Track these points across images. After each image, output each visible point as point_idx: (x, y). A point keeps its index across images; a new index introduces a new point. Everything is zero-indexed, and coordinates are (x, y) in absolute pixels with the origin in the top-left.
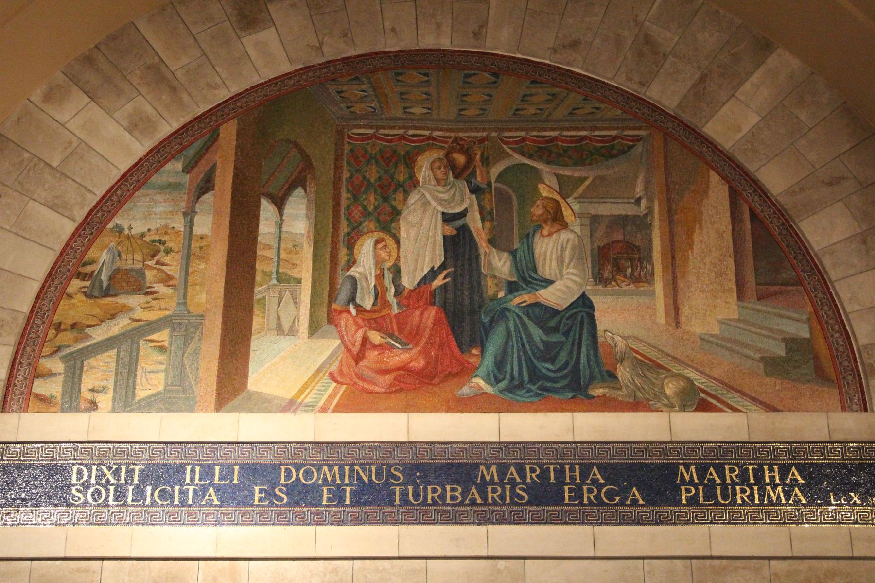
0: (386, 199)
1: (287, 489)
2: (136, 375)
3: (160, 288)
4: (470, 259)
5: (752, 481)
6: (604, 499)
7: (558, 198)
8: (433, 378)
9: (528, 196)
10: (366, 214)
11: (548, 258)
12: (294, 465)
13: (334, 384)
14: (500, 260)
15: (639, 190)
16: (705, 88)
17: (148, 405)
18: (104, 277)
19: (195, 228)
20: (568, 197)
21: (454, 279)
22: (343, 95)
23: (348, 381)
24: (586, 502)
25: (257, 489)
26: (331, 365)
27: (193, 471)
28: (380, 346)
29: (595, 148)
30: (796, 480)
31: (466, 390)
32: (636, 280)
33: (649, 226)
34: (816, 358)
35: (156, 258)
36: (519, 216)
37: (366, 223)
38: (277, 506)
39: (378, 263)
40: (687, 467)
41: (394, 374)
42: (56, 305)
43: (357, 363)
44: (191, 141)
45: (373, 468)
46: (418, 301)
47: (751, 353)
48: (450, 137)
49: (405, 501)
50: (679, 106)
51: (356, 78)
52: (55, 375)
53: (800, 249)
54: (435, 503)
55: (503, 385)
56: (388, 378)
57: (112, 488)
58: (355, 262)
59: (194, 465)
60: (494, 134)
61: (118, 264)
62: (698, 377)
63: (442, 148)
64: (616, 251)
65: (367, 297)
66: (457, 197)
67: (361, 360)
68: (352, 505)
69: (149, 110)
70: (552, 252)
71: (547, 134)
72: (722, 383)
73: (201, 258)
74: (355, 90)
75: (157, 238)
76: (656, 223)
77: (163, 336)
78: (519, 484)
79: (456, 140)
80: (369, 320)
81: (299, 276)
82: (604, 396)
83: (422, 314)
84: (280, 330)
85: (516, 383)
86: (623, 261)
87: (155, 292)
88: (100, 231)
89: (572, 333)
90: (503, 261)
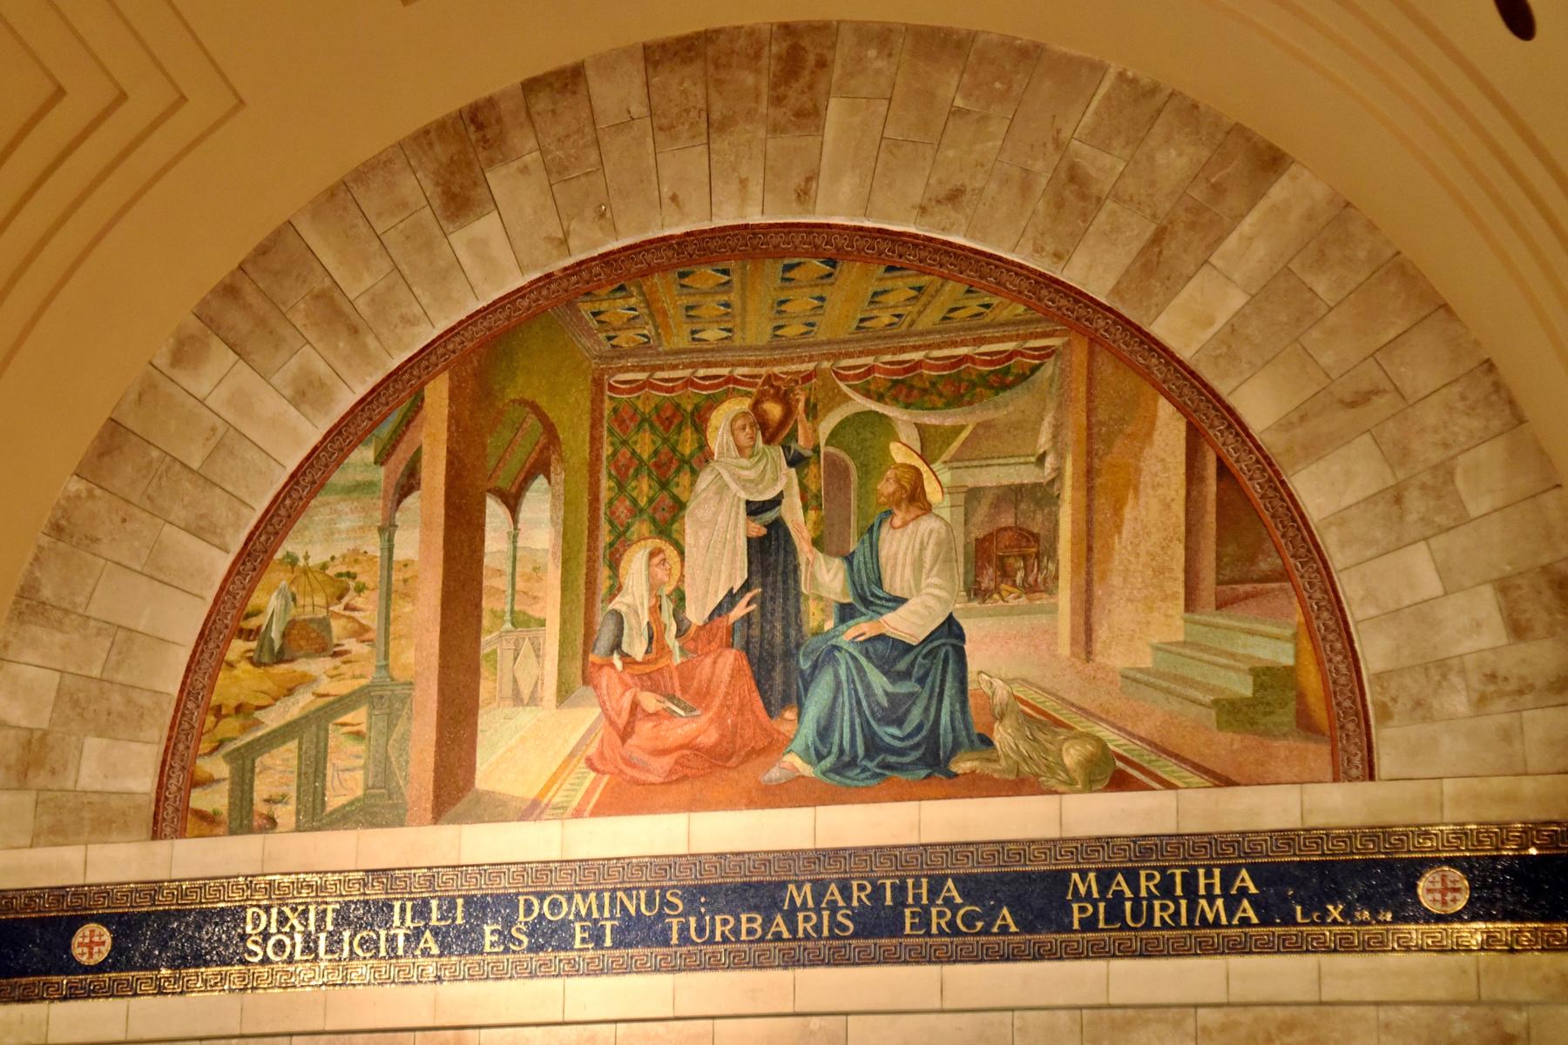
0: (664, 485)
3: (351, 645)
5: (1179, 892)
7: (919, 463)
8: (729, 758)
10: (636, 511)
11: (900, 562)
12: (536, 894)
15: (1044, 441)
16: (1160, 252)
17: (344, 819)
20: (934, 461)
21: (762, 606)
22: (602, 318)
23: (611, 768)
24: (934, 930)
28: (656, 714)
32: (1030, 589)
33: (1055, 500)
34: (1301, 697)
35: (345, 601)
36: (860, 499)
39: (654, 587)
41: (675, 755)
42: (214, 678)
43: (624, 741)
45: (643, 894)
47: (1199, 695)
48: (759, 376)
49: (685, 939)
51: (622, 288)
52: (218, 781)
55: (828, 763)
56: (667, 761)
58: (620, 589)
60: (826, 365)
61: (293, 612)
63: (748, 394)
65: (637, 641)
66: (769, 475)
69: (322, 367)
72: (1150, 743)
73: (406, 596)
75: (344, 569)
76: (1067, 494)
77: (358, 717)
79: (769, 379)
81: (542, 616)
82: (973, 772)
83: (715, 662)
84: (517, 699)
85: (846, 758)
86: (1011, 560)
87: (346, 652)
88: (265, 565)
89: (930, 679)
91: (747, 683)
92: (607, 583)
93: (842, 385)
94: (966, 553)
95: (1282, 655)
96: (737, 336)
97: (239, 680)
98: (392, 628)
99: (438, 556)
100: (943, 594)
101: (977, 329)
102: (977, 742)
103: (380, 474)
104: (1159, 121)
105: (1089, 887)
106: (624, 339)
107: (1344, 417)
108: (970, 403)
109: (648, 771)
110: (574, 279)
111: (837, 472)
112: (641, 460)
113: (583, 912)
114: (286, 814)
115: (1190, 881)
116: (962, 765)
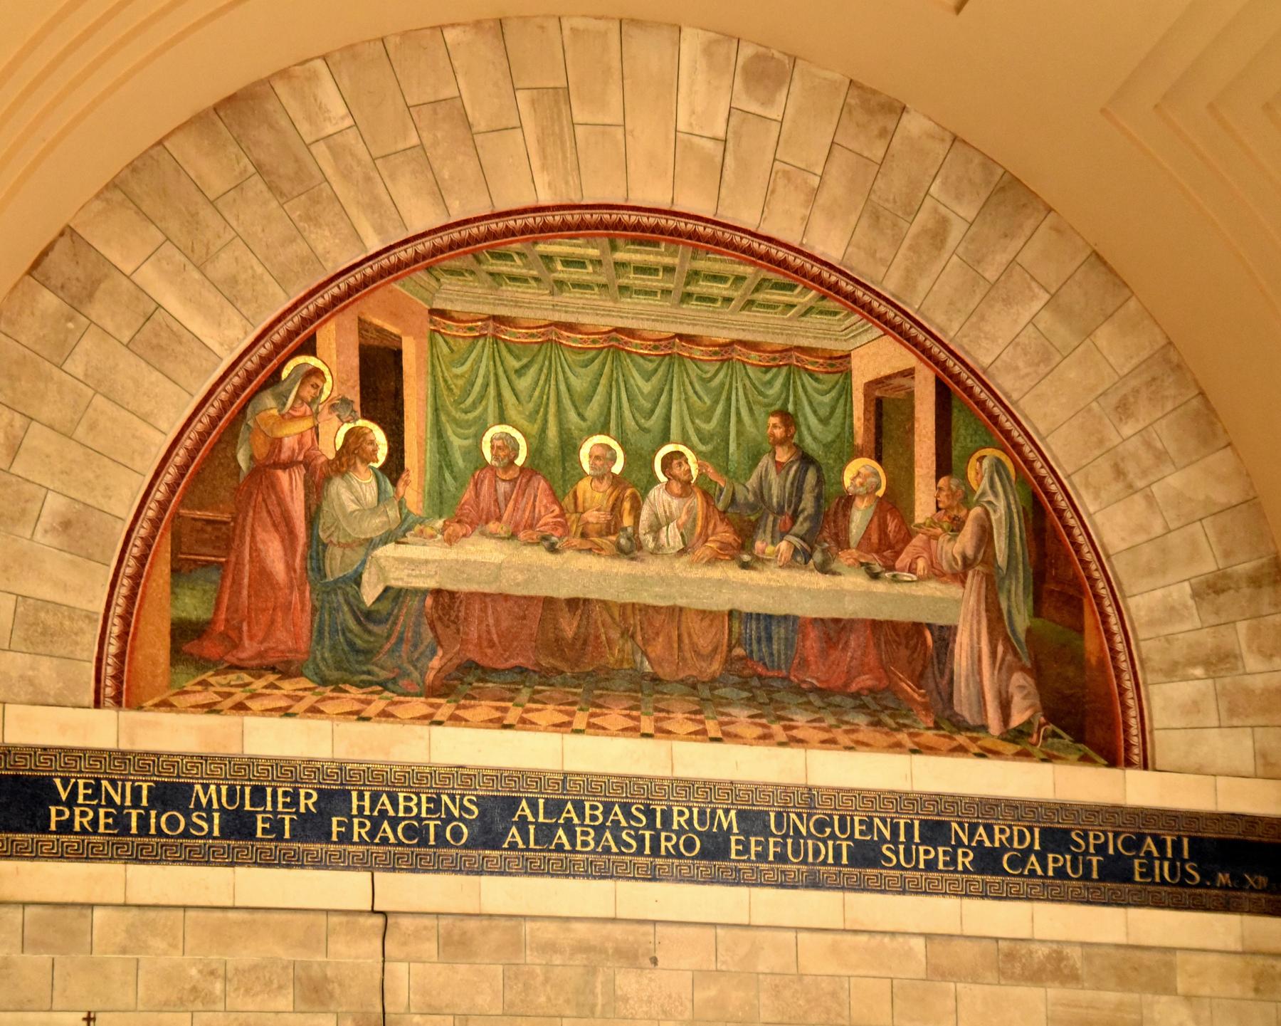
24: (960, 868)
25: (334, 820)
56: (553, 681)
59: (123, 781)
105: (730, 823)
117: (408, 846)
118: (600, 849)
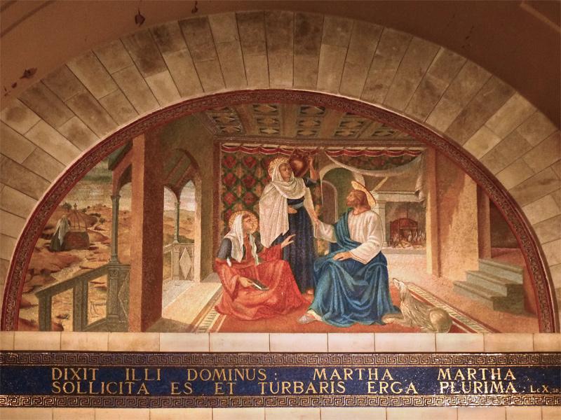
0: (249, 189)
1: (192, 384)
2: (87, 307)
3: (99, 245)
4: (306, 229)
5: (484, 379)
6: (393, 390)
7: (364, 190)
8: (283, 310)
9: (344, 189)
10: (236, 199)
11: (357, 229)
12: (196, 368)
13: (219, 314)
14: (326, 229)
15: (418, 186)
16: (465, 119)
17: (96, 328)
18: (60, 237)
19: (120, 207)
20: (371, 190)
21: (296, 242)
22: (217, 119)
23: (228, 312)
24: (381, 392)
25: (173, 384)
26: (216, 300)
27: (130, 372)
28: (248, 288)
29: (390, 158)
30: (511, 377)
31: (304, 319)
32: (414, 243)
33: (424, 210)
34: (526, 298)
35: (95, 225)
36: (339, 202)
37: (236, 206)
38: (186, 395)
39: (245, 230)
40: (444, 369)
41: (257, 308)
42: (29, 256)
43: (233, 300)
44: (115, 151)
45: (247, 370)
46: (272, 256)
47: (486, 295)
48: (292, 150)
49: (268, 392)
50: (448, 131)
51: (227, 108)
52: (33, 306)
53: (520, 224)
54: (286, 393)
55: (328, 315)
56: (253, 311)
57: (78, 383)
58: (229, 230)
60: (322, 148)
61: (69, 228)
62: (451, 311)
63: (287, 156)
64: (401, 225)
65: (238, 252)
66: (297, 189)
67: (236, 298)
68: (234, 394)
69: (83, 126)
70: (360, 225)
71: (356, 148)
72: (467, 314)
73: (125, 226)
74: (226, 117)
75: (94, 212)
76: (429, 207)
77: (103, 279)
78: (340, 380)
79: (296, 151)
80: (240, 270)
81: (192, 238)
82: (392, 323)
83: (275, 266)
84: (181, 276)
85: (336, 314)
86: (406, 231)
87: (96, 248)
88: (55, 207)
89: (372, 280)
90: (327, 231)
91: (290, 277)
92: (223, 227)
93: (329, 156)
94: (386, 227)
95: (519, 280)
96: (282, 132)
97: (43, 257)
98: (119, 239)
99: (141, 210)
100: (377, 243)
101: (388, 141)
102: (394, 310)
103: (112, 174)
104: (462, 70)
106: (229, 129)
107: (540, 187)
108: (386, 169)
109: (245, 314)
110: (204, 103)
111: (328, 191)
112: (238, 179)
113: (444, 376)
114: (68, 324)
115: (488, 375)
116: (388, 320)
117: (112, 395)
118: (307, 392)
